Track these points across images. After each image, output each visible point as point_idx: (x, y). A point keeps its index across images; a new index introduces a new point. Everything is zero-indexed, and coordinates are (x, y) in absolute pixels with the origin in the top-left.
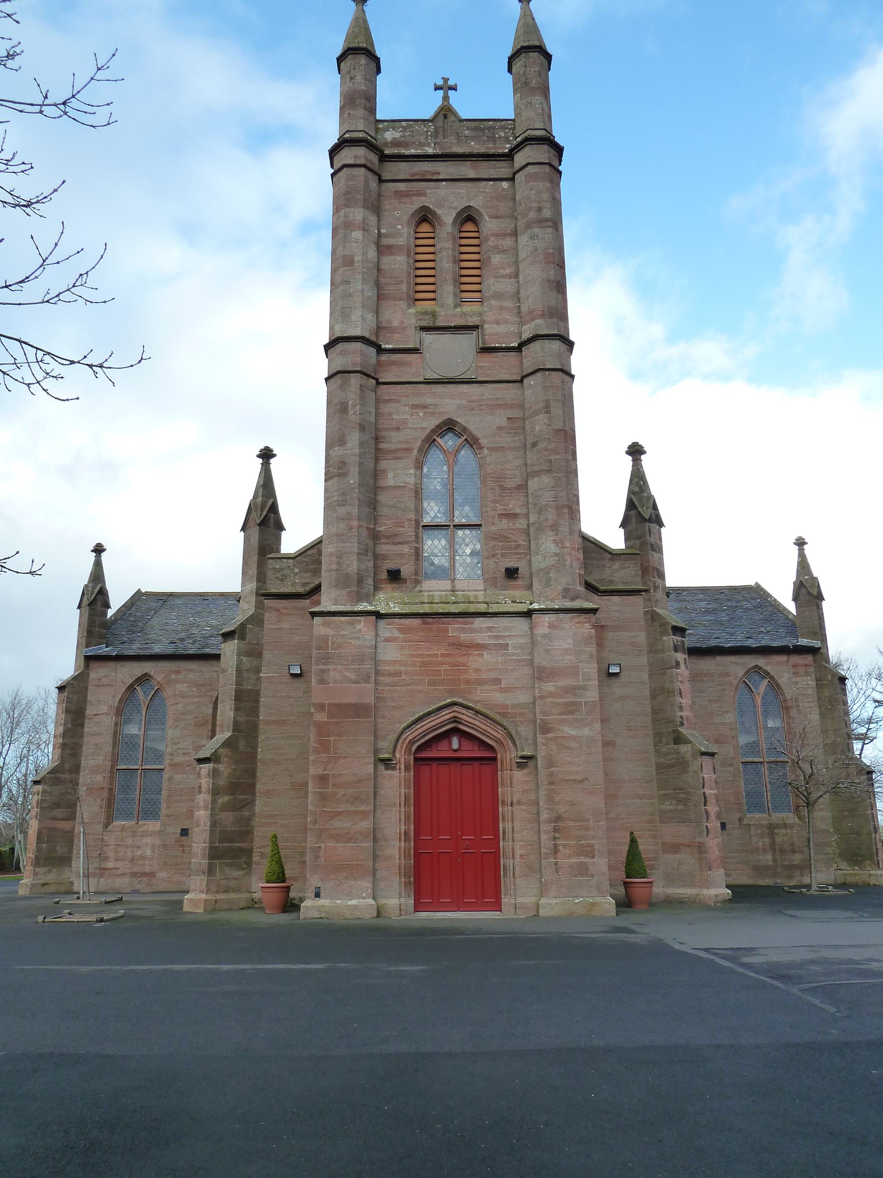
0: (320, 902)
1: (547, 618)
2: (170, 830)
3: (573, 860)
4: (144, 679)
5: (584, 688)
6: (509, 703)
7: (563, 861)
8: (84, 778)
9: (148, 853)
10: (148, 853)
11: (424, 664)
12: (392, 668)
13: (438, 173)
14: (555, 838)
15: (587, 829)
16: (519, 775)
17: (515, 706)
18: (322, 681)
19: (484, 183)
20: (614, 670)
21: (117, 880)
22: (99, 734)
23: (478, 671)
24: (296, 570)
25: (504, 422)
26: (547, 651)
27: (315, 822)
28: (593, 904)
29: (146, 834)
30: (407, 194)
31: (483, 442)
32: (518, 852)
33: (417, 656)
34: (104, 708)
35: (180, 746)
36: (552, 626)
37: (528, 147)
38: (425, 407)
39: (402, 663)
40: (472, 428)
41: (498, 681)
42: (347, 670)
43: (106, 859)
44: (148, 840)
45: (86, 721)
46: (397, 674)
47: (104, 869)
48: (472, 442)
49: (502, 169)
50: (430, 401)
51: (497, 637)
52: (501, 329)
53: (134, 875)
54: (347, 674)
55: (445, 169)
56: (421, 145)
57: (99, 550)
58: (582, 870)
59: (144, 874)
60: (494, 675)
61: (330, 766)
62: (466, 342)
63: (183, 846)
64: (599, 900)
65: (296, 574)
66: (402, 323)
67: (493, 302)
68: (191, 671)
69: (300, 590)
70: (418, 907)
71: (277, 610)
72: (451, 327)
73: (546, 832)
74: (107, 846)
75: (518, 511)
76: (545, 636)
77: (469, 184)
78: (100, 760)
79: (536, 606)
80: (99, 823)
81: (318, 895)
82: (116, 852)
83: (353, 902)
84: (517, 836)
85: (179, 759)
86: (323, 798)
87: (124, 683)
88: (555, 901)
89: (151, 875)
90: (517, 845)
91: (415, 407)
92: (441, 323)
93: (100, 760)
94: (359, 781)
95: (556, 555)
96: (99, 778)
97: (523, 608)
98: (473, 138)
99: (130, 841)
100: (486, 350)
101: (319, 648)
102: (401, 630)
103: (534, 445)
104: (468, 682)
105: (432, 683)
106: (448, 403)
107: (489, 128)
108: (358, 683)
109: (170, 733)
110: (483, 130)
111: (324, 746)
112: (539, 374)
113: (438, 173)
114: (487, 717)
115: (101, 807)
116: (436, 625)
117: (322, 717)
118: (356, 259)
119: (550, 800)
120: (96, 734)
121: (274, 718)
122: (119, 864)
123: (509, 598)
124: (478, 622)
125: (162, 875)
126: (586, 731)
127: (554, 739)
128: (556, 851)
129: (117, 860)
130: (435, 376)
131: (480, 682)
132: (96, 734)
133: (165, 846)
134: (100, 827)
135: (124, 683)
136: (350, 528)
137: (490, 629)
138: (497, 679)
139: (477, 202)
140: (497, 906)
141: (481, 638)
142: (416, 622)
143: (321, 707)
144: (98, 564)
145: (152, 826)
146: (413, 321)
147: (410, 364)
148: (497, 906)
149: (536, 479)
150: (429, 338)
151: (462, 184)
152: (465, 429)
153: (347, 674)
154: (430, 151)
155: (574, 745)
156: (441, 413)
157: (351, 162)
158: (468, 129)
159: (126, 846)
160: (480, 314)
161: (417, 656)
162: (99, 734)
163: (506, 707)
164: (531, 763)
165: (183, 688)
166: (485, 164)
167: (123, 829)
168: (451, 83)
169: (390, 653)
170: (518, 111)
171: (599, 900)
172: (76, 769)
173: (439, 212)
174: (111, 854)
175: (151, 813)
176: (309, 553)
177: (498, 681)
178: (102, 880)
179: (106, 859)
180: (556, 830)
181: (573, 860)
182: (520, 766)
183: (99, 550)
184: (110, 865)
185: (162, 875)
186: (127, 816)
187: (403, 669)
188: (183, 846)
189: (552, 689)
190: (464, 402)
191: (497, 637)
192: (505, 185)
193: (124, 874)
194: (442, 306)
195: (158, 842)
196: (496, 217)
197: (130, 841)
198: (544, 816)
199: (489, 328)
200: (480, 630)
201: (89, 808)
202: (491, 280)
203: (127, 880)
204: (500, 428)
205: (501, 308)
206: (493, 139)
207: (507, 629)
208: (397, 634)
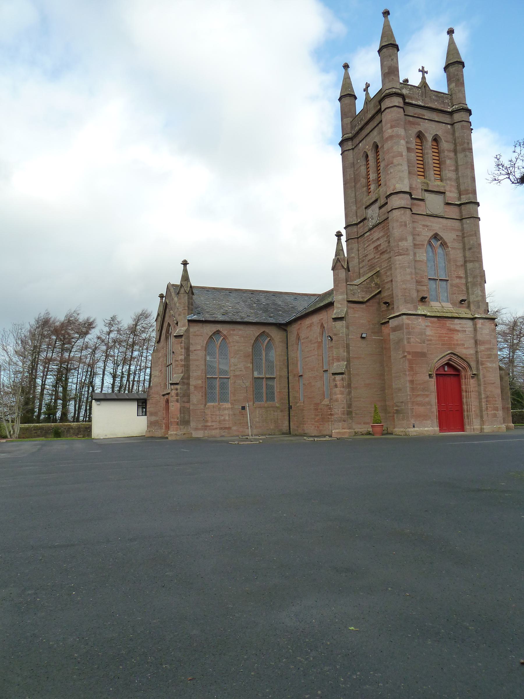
0: (416, 429)
1: (481, 321)
2: (236, 407)
3: (492, 412)
4: (218, 332)
5: (493, 348)
6: (467, 353)
7: (490, 413)
8: (193, 382)
9: (227, 418)
10: (227, 418)
11: (440, 337)
12: (429, 338)
13: (424, 115)
14: (487, 404)
15: (496, 401)
16: (472, 381)
17: (469, 355)
18: (408, 342)
19: (441, 124)
20: (364, 335)
21: (213, 431)
22: (197, 360)
23: (457, 340)
24: (359, 291)
25: (455, 237)
26: (481, 334)
27: (411, 399)
28: (499, 428)
29: (225, 409)
30: (413, 123)
31: (449, 245)
32: (473, 410)
33: (437, 333)
34: (199, 347)
35: (239, 366)
36: (482, 324)
37: (462, 112)
38: (427, 226)
39: (432, 336)
40: (444, 238)
41: (463, 345)
42: (417, 338)
43: (207, 421)
44: (226, 412)
45: (190, 353)
46: (431, 340)
47: (207, 426)
48: (444, 245)
49: (446, 119)
50: (429, 224)
51: (463, 327)
52: (452, 195)
53: (221, 429)
54: (417, 340)
55: (428, 114)
56: (417, 100)
57: (185, 263)
58: (495, 416)
59: (226, 428)
60: (462, 342)
61: (414, 376)
62: (439, 199)
63: (243, 414)
64: (501, 426)
65: (359, 292)
66: (416, 186)
67: (448, 182)
68: (240, 330)
69: (361, 300)
70: (441, 430)
71: (353, 308)
72: (435, 191)
73: (484, 402)
74: (207, 415)
75: (462, 276)
76: (480, 328)
77: (436, 123)
78: (199, 373)
79: (476, 316)
80: (202, 404)
81: (414, 427)
82: (211, 418)
83: (426, 429)
84: (473, 404)
85: (238, 373)
86: (413, 389)
87: (207, 334)
88: (488, 427)
89: (229, 428)
90: (473, 407)
91: (424, 225)
92: (430, 189)
93: (199, 373)
94: (424, 382)
95: (481, 296)
96: (200, 382)
97: (470, 316)
98: (437, 101)
99: (218, 413)
100: (448, 204)
101: (406, 329)
102: (431, 322)
103: (470, 249)
104: (454, 344)
105: (443, 345)
106: (437, 226)
107: (442, 97)
108: (421, 343)
109: (232, 360)
110: (440, 97)
111: (411, 369)
112: (472, 219)
113: (424, 115)
114: (462, 359)
115: (202, 396)
116: (443, 321)
117: (409, 357)
118: (404, 154)
119: (485, 390)
120: (196, 360)
121: (356, 356)
122: (213, 424)
123: (463, 312)
124: (457, 321)
125: (234, 428)
126: (494, 365)
127: (485, 368)
128: (487, 409)
129: (212, 422)
130: (430, 213)
131: (458, 345)
132: (196, 360)
133: (234, 414)
134: (202, 406)
135: (207, 334)
136: (412, 279)
137: (460, 324)
138: (217, 331)
139: (440, 133)
140: (463, 429)
141: (458, 327)
142: (436, 319)
143: (409, 353)
144: (185, 271)
145: (228, 405)
146: (420, 186)
147: (419, 205)
148: (463, 429)
149: (471, 264)
150: (427, 195)
151: (434, 123)
152: (441, 238)
153: (417, 340)
154: (420, 103)
155: (491, 370)
156: (433, 230)
157: (397, 105)
158: (434, 95)
159: (216, 415)
160: (444, 187)
161: (437, 333)
162: (197, 360)
163: (467, 355)
164: (476, 377)
165: (237, 338)
166: (441, 115)
167: (213, 407)
168: (425, 70)
169: (429, 332)
170: (387, 63)
171: (501, 426)
172: (188, 378)
173: (426, 135)
174: (209, 419)
175: (223, 399)
176: (363, 283)
177: (463, 345)
178: (206, 431)
179: (207, 421)
180: (487, 401)
181: (492, 412)
182: (472, 377)
183: (185, 263)
184: (209, 424)
185: (234, 428)
186: (213, 401)
187: (432, 338)
188: (243, 414)
189: (483, 349)
190: (441, 226)
191: (463, 327)
192: (449, 126)
193: (216, 428)
194: (430, 180)
195: (231, 413)
196: (447, 142)
197: (218, 413)
198: (483, 396)
199: (448, 194)
200: (457, 324)
201: (196, 397)
202: (447, 172)
203: (218, 431)
204: (454, 239)
205: (451, 185)
206: (443, 103)
207: (466, 324)
208: (430, 324)
